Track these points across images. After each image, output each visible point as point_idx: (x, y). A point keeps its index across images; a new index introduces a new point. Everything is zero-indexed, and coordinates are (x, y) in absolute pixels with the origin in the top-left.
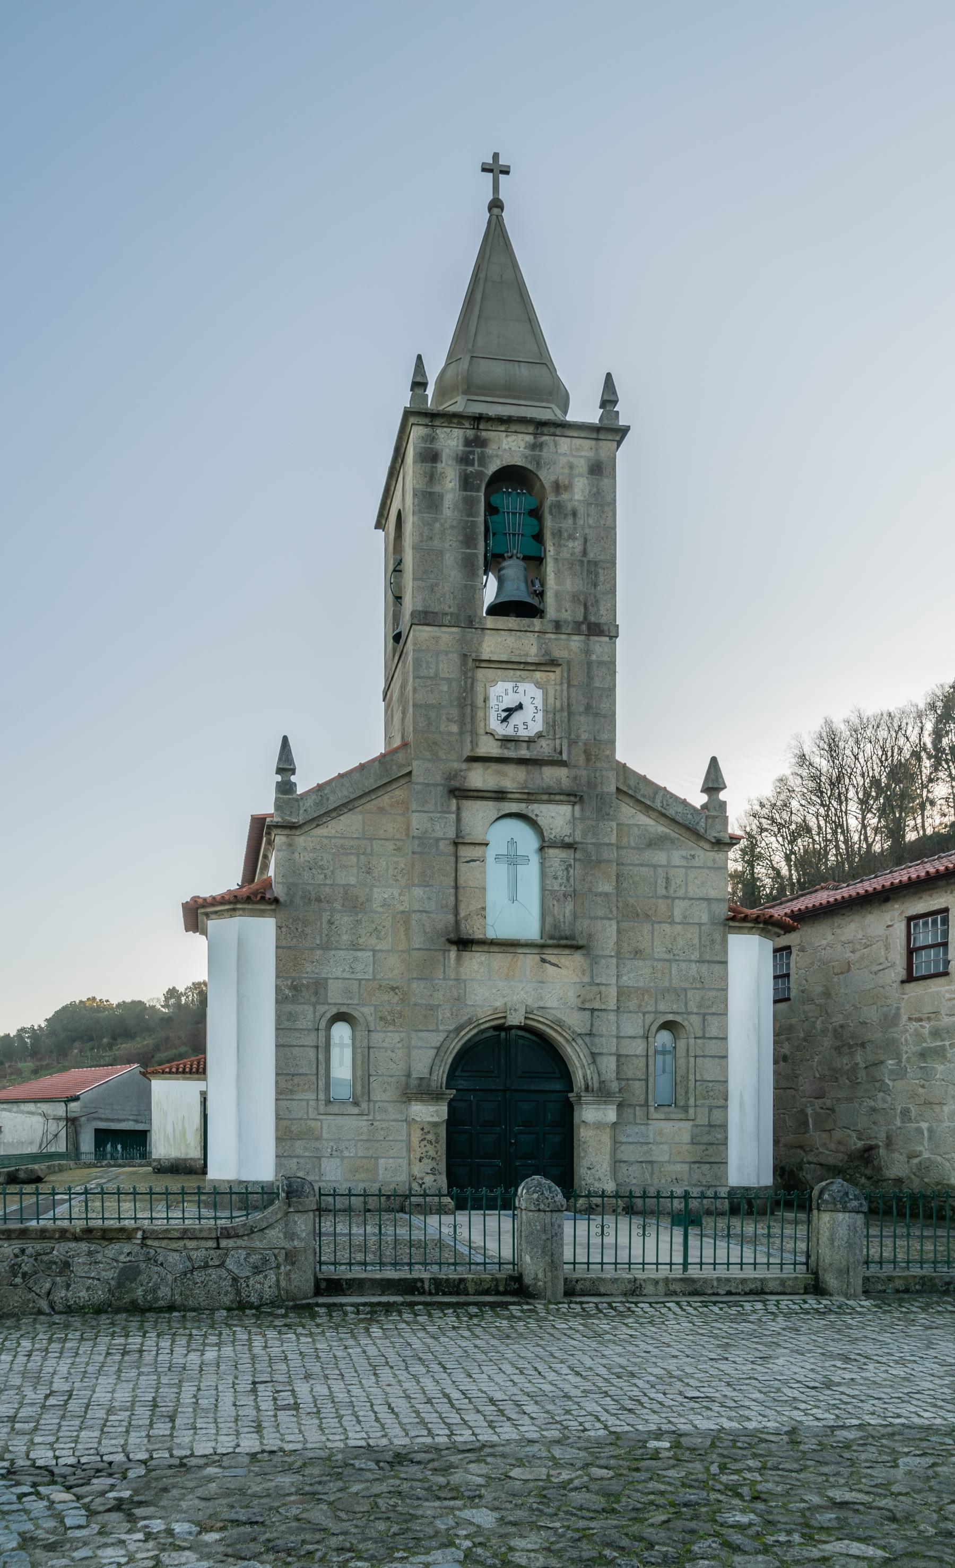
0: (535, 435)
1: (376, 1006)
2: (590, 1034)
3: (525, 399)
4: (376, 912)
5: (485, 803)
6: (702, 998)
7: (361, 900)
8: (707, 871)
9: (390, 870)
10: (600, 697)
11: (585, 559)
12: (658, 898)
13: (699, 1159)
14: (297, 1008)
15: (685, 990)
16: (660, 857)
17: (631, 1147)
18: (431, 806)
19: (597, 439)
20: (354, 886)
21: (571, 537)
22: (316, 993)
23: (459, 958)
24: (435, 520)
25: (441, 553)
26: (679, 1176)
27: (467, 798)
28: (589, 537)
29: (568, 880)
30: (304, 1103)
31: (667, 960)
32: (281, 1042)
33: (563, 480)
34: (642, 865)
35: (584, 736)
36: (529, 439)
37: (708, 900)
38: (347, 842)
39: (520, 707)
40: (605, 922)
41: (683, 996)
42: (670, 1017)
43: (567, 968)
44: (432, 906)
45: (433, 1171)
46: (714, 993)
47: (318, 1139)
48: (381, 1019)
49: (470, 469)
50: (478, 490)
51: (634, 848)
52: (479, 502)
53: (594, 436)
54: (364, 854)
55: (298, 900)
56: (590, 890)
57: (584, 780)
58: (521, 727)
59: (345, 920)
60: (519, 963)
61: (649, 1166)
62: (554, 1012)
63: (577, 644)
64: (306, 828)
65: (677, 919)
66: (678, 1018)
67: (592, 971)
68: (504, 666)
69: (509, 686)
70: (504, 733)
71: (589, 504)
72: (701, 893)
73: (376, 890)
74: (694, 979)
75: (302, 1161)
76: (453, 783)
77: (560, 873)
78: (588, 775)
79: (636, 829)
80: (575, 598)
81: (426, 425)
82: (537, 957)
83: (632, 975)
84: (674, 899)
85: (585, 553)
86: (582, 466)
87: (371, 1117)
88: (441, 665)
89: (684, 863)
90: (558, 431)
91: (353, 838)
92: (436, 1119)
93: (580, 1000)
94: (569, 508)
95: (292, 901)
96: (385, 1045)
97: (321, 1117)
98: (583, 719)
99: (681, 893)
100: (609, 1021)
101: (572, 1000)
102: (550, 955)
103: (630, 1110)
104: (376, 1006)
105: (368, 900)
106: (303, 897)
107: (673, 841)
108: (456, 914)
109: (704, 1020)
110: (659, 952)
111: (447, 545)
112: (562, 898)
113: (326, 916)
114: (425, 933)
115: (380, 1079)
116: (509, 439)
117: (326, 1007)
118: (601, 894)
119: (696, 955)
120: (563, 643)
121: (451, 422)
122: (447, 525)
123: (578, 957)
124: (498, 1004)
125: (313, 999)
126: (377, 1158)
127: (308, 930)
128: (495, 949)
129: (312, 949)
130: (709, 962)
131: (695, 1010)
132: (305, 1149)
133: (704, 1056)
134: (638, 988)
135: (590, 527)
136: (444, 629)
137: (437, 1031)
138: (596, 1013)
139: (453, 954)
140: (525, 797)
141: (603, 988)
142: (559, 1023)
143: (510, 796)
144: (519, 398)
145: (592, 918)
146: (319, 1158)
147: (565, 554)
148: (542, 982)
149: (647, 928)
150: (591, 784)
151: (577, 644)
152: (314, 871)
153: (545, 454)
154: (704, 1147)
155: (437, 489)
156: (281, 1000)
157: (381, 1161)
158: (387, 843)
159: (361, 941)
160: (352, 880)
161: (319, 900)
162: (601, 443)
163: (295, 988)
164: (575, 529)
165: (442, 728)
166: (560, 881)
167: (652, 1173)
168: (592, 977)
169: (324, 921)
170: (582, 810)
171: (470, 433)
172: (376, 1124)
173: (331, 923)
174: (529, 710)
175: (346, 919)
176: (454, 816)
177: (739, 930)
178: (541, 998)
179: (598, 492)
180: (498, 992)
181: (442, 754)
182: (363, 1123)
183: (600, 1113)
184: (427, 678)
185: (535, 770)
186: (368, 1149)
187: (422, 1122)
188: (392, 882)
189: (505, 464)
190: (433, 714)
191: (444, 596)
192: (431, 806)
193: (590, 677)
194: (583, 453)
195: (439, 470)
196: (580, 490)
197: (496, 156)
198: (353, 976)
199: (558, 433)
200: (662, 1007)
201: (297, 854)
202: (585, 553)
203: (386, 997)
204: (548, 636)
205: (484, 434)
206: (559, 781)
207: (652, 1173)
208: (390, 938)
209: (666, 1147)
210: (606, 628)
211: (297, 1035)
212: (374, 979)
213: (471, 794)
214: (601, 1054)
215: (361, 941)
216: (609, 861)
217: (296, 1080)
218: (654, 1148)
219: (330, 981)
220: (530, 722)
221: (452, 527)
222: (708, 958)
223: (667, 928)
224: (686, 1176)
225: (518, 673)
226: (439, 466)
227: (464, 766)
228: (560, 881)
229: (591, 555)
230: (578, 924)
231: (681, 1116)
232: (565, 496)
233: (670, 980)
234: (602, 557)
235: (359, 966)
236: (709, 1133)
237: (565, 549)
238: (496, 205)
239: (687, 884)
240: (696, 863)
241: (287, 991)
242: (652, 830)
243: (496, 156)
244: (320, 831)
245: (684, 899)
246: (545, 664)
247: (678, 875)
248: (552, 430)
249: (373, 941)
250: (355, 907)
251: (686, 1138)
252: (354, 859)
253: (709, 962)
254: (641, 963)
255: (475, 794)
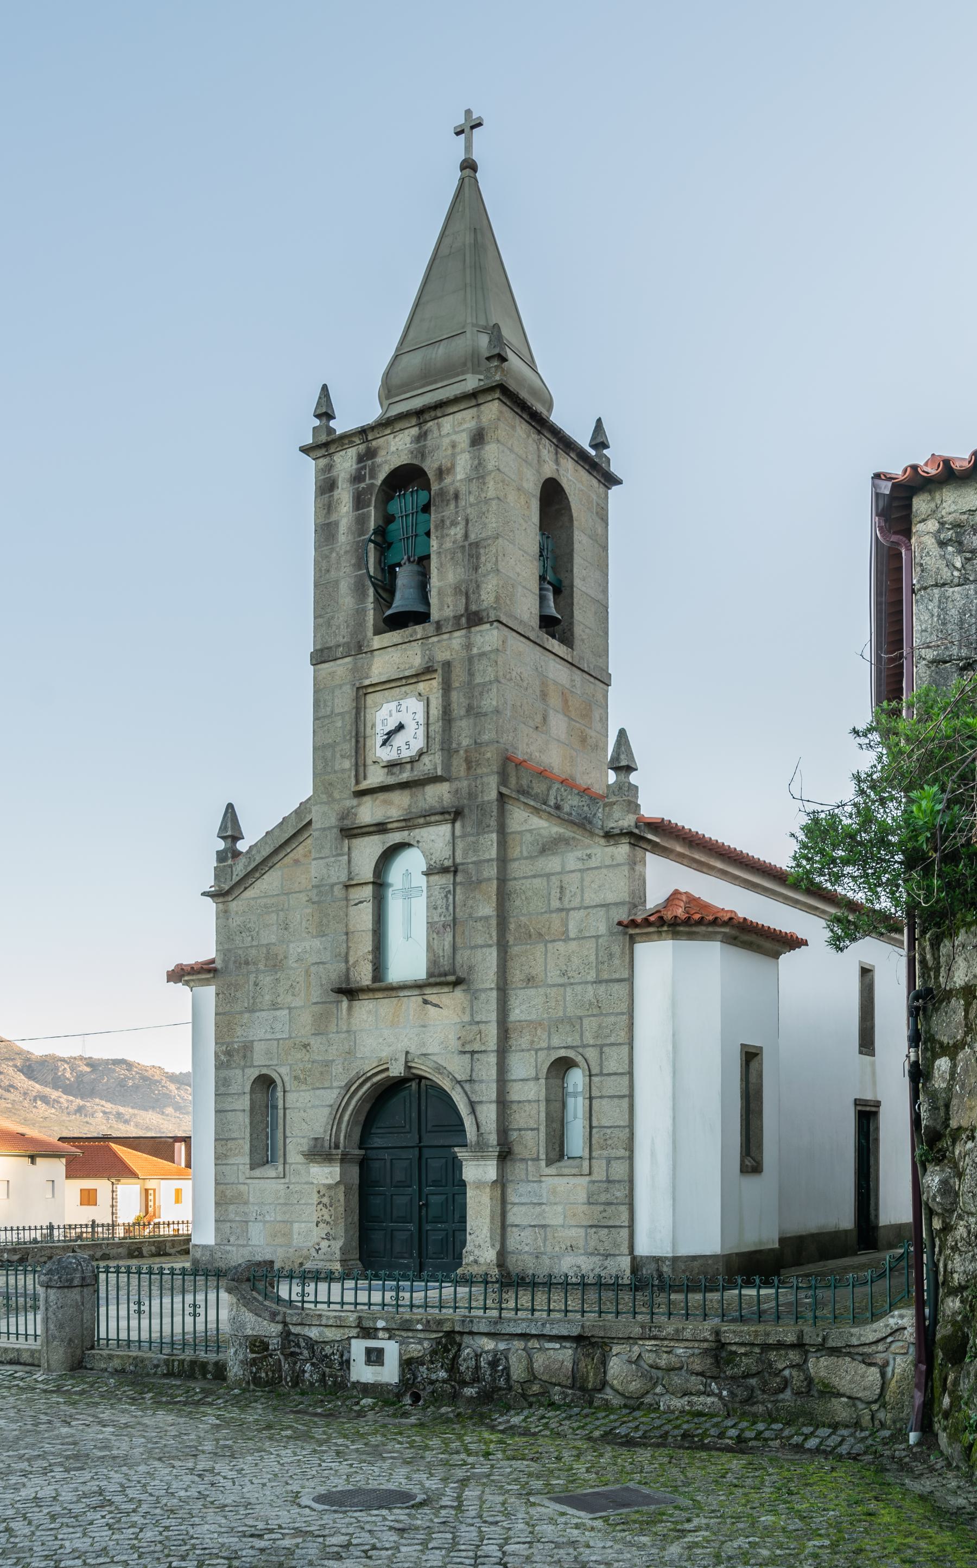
0: (419, 425)
1: (291, 1065)
2: (471, 1081)
3: (442, 380)
4: (292, 968)
5: (372, 837)
6: (600, 1026)
7: (279, 958)
8: (604, 871)
9: (304, 923)
10: (481, 694)
11: (466, 543)
12: (551, 912)
13: (596, 1223)
14: (230, 1073)
15: (580, 1018)
16: (552, 863)
17: (523, 1209)
18: (326, 852)
19: (478, 405)
20: (274, 944)
21: (454, 524)
22: (245, 1057)
23: (350, 1008)
24: (332, 550)
25: (337, 582)
26: (574, 1243)
27: (355, 836)
28: (471, 517)
29: (447, 909)
30: (235, 1168)
31: (561, 985)
32: (219, 1107)
33: (446, 463)
34: (534, 876)
35: (465, 742)
36: (415, 431)
37: (606, 906)
38: (268, 901)
39: (401, 727)
40: (484, 950)
41: (578, 1027)
42: (562, 1053)
43: (448, 1007)
44: (326, 956)
45: (328, 1237)
46: (612, 1019)
47: (246, 1203)
48: (296, 1078)
49: (363, 485)
50: (369, 506)
51: (526, 858)
52: (369, 517)
53: (473, 403)
54: (282, 910)
55: (231, 966)
56: (470, 916)
57: (465, 792)
58: (404, 747)
59: (266, 980)
60: (404, 1007)
61: (542, 1232)
62: (434, 1058)
63: (459, 641)
64: (236, 892)
65: (572, 935)
66: (571, 1054)
67: (472, 1007)
68: (388, 686)
69: (393, 706)
70: (389, 758)
71: (471, 480)
72: (598, 901)
73: (291, 945)
74: (591, 1004)
75: (234, 1225)
76: (346, 822)
77: (439, 902)
78: (469, 785)
79: (528, 835)
80: (457, 590)
81: (324, 456)
82: (420, 999)
83: (524, 1007)
84: (568, 910)
85: (466, 536)
86: (463, 440)
87: (287, 1181)
88: (336, 700)
89: (580, 865)
90: (439, 413)
91: (273, 896)
92: (330, 1181)
93: (460, 1042)
94: (452, 491)
95: (226, 967)
96: (298, 1105)
97: (249, 1181)
98: (464, 723)
99: (576, 903)
100: (488, 1063)
101: (454, 1044)
102: (432, 995)
103: (523, 1166)
104: (291, 1065)
105: (285, 958)
106: (235, 962)
107: (567, 841)
108: (347, 962)
109: (601, 1053)
110: (554, 976)
111: (341, 574)
112: (442, 930)
113: (252, 978)
114: (322, 985)
115: (295, 1140)
116: (397, 439)
117: (252, 1069)
118: (481, 919)
119: (592, 976)
120: (444, 643)
121: (343, 445)
122: (342, 552)
123: (459, 993)
124: (384, 1054)
125: (242, 1063)
126: (292, 1223)
127: (238, 994)
128: (379, 995)
129: (241, 1013)
130: (607, 981)
131: (591, 1042)
132: (237, 1213)
133: (601, 1097)
134: (531, 1022)
135: (471, 505)
136: (339, 662)
137: (331, 1088)
138: (476, 1056)
139: (345, 1004)
140: (403, 824)
141: (482, 1026)
142: (439, 1069)
143: (389, 826)
144: (435, 382)
145: (472, 948)
146: (246, 1222)
147: (448, 544)
148: (424, 1026)
149: (541, 947)
150: (472, 795)
151: (459, 641)
152: (243, 934)
153: (429, 443)
154: (601, 1208)
155: (334, 518)
156: (219, 1066)
157: (296, 1225)
158: (301, 895)
159: (279, 1000)
160: (273, 939)
161: (247, 963)
162: (482, 407)
163: (229, 1053)
164: (457, 513)
165: (337, 767)
166: (439, 910)
167: (545, 1240)
168: (472, 1015)
169: (251, 983)
170: (463, 826)
171: (362, 448)
172: (291, 1186)
173: (256, 984)
174: (411, 727)
175: (268, 978)
176: (346, 857)
177: (647, 937)
178: (424, 1044)
179: (480, 464)
180: (387, 1038)
181: (337, 795)
182: (279, 1186)
183: (480, 1170)
184: (324, 717)
185: (418, 791)
186: (284, 1213)
187: (318, 1185)
188: (304, 935)
189: (393, 467)
190: (329, 754)
191: (338, 627)
192: (326, 852)
193: (471, 674)
194: (465, 426)
195: (335, 498)
196: (463, 467)
197: (468, 112)
198: (273, 1036)
199: (439, 414)
200: (556, 1042)
201: (230, 920)
202: (466, 536)
203: (299, 1056)
204: (431, 640)
205: (374, 443)
206: (441, 799)
207: (545, 1240)
208: (302, 994)
209: (559, 1208)
210: (485, 614)
211: (230, 1099)
212: (290, 1038)
213: (356, 831)
214: (481, 1102)
215: (279, 1000)
216: (489, 879)
217: (230, 1144)
218: (547, 1208)
219: (255, 1043)
220: (411, 742)
221: (346, 552)
222: (606, 977)
223: (560, 946)
224: (581, 1243)
225: (403, 689)
226: (336, 493)
227: (355, 802)
228: (439, 910)
229: (472, 537)
230: (458, 957)
231: (574, 1171)
232: (448, 480)
233: (565, 1007)
234: (483, 535)
235: (278, 1026)
236: (607, 1190)
237: (448, 539)
238: (469, 166)
239: (582, 892)
240: (593, 863)
241: (222, 1057)
242: (545, 833)
243: (468, 112)
244: (249, 894)
245: (579, 909)
246: (423, 673)
247: (572, 882)
248: (433, 414)
249: (289, 998)
250: (275, 966)
251: (582, 1196)
252: (274, 916)
253: (607, 981)
254: (532, 992)
255: (359, 831)
